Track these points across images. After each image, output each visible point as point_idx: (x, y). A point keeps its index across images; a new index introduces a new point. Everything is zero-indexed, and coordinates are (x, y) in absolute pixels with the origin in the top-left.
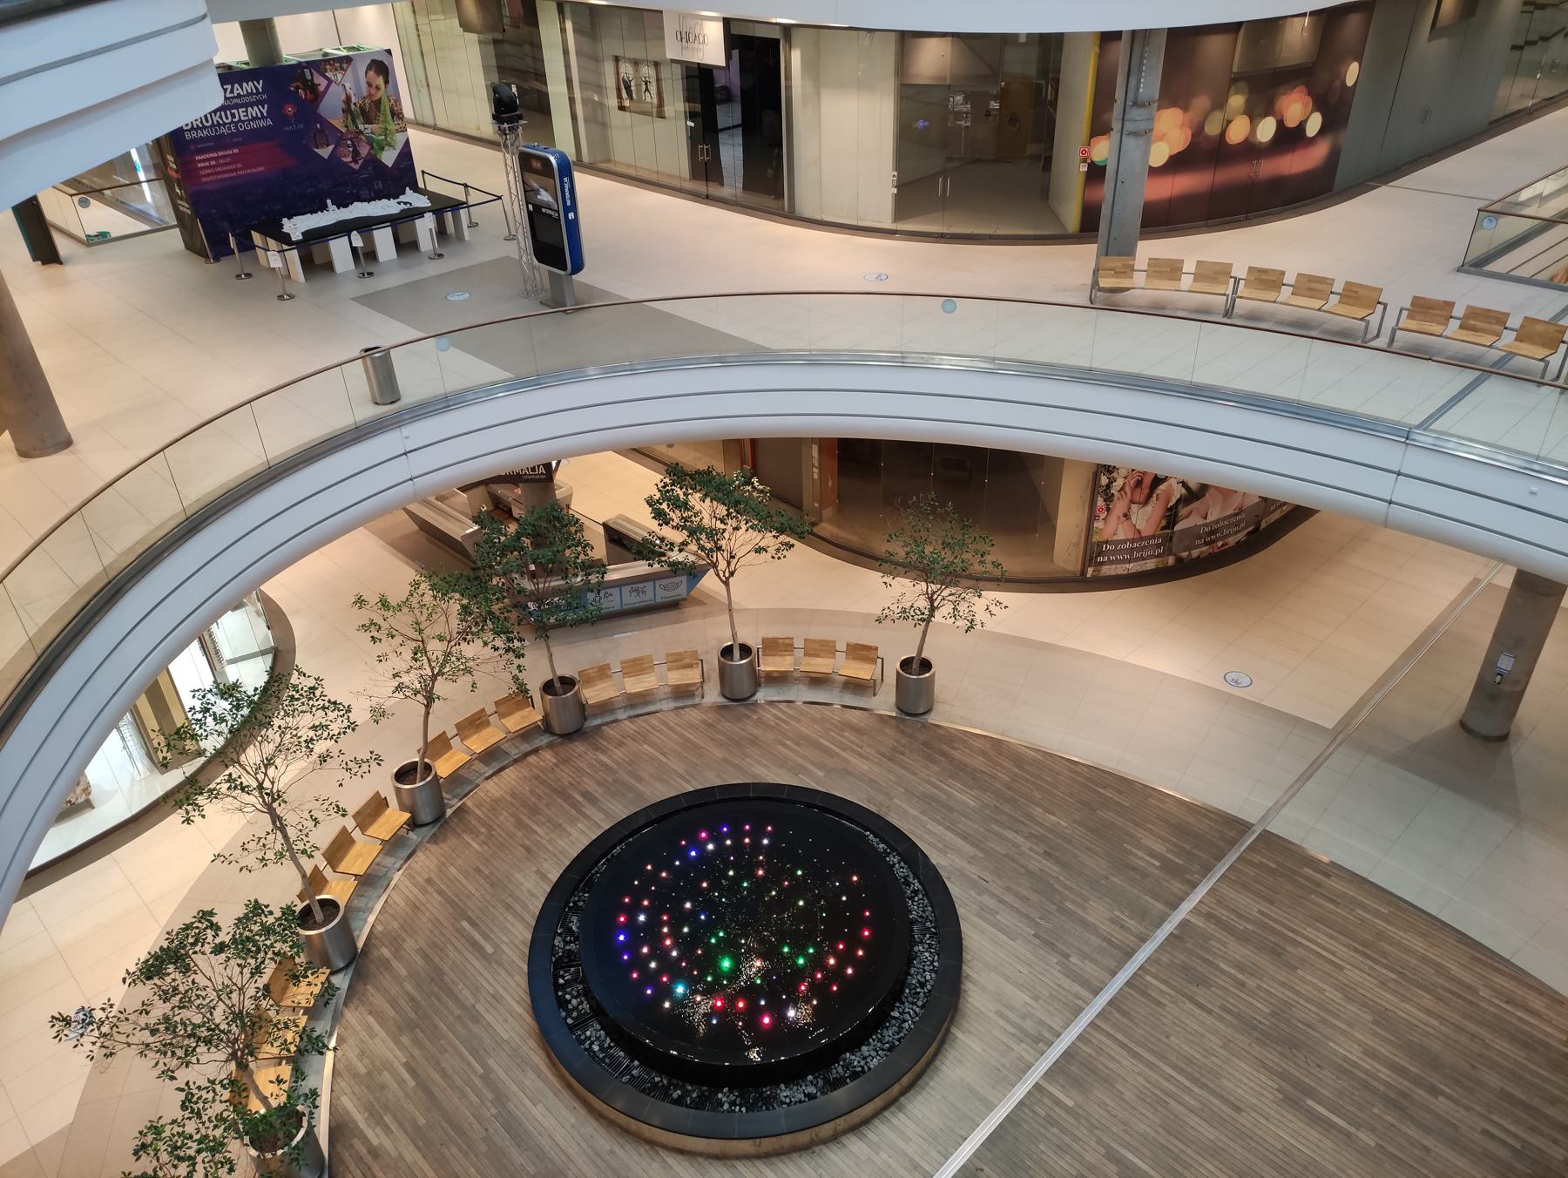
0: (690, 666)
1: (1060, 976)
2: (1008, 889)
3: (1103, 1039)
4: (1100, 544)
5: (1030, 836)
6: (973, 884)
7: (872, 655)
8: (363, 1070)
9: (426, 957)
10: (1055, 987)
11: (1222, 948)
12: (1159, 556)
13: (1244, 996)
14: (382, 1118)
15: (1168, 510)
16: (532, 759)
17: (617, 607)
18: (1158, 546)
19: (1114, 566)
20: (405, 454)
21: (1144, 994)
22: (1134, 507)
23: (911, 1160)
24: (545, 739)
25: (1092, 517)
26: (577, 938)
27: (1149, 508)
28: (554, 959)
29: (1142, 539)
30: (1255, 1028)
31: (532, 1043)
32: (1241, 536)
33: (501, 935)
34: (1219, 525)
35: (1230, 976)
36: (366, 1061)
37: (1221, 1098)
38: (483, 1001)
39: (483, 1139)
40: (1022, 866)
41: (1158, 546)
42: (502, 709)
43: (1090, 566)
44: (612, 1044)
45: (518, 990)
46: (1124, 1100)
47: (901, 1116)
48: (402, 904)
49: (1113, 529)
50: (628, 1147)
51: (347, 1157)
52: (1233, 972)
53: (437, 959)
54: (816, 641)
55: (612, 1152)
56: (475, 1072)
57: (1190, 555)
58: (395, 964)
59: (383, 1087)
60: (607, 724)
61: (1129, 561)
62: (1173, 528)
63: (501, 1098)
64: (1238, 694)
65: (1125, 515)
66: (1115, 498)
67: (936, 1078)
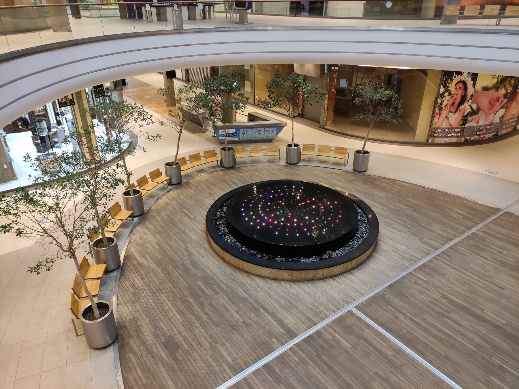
0: (275, 151)
1: (420, 243)
2: (398, 218)
3: (440, 262)
4: (435, 129)
5: (407, 205)
6: (383, 216)
7: (344, 151)
8: (140, 242)
9: (168, 216)
10: (418, 246)
11: (491, 242)
12: (458, 137)
13: (502, 256)
14: (145, 255)
15: (464, 117)
16: (215, 173)
17: (250, 138)
18: (458, 132)
19: (440, 139)
20: (183, 45)
21: (457, 251)
22: (450, 114)
23: (355, 289)
24: (221, 169)
25: (433, 117)
26: (225, 213)
27: (456, 115)
28: (216, 218)
29: (452, 128)
30: (508, 266)
31: (204, 241)
32: (491, 135)
33: (197, 213)
34: (483, 128)
35: (495, 249)
36: (142, 240)
37: (495, 285)
38: (188, 229)
39: (182, 265)
40: (403, 213)
41: (458, 132)
42: (206, 155)
43: (430, 138)
44: (236, 241)
45: (201, 228)
46: (450, 281)
47: (351, 276)
48: (163, 203)
49: (441, 123)
50: (238, 273)
51: (129, 264)
52: (497, 249)
53: (172, 217)
54: (323, 146)
55: (232, 273)
56: (182, 247)
57: (470, 139)
58: (157, 217)
59: (147, 247)
60: (243, 167)
61: (446, 137)
62: (465, 125)
63: (190, 254)
64: (493, 175)
65: (446, 117)
66: (443, 109)
67: (366, 266)
